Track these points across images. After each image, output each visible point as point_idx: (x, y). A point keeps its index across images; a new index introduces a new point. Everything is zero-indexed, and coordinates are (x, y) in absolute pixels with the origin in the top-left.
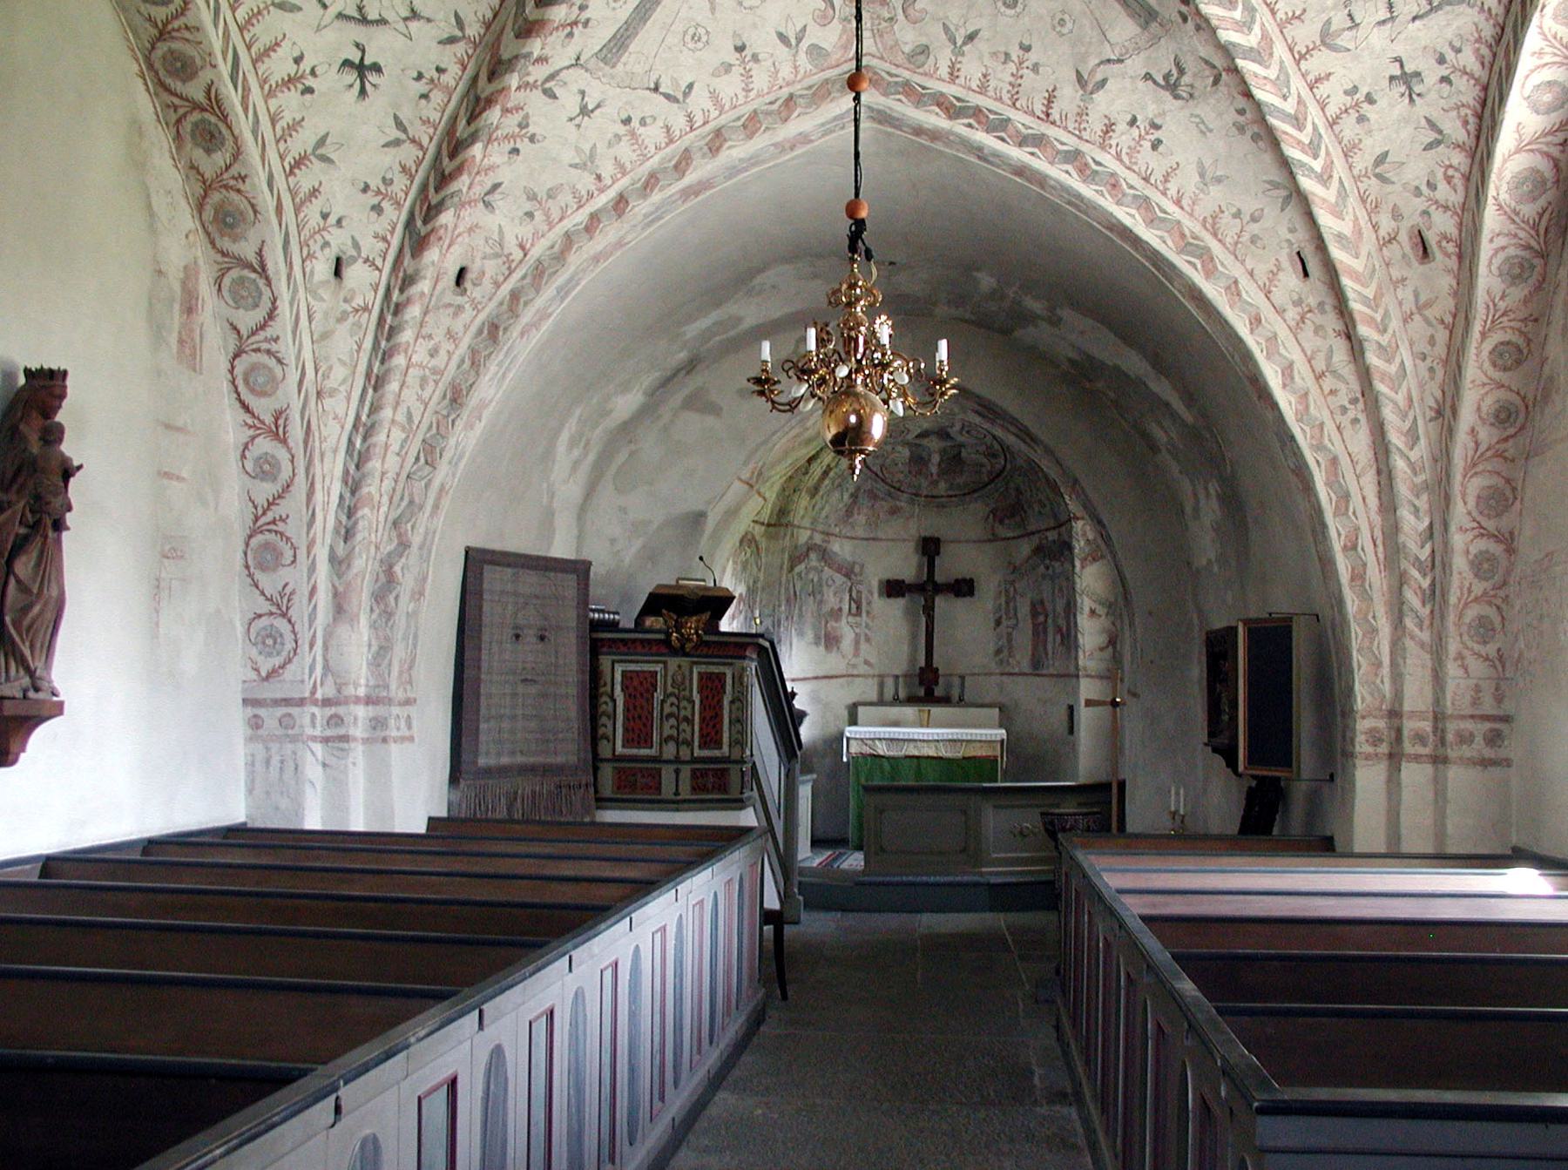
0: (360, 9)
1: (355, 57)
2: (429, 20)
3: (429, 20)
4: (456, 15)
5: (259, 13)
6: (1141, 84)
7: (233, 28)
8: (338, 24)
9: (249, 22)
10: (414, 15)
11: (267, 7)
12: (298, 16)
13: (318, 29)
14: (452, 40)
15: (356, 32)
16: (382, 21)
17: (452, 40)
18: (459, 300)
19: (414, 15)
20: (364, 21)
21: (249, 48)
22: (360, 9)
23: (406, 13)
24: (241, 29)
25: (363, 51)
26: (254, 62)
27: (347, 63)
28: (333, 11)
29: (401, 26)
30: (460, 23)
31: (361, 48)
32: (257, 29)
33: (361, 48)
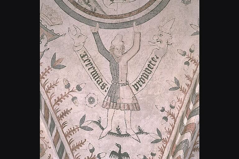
0: (118, 130)
1: (117, 150)
2: (147, 133)
3: (147, 133)
4: (158, 130)
5: (74, 130)
6: (79, 39)
7: (56, 120)
8: (110, 136)
9: (62, 116)
10: (141, 132)
11: (78, 128)
12: (92, 132)
13: (100, 138)
14: (157, 141)
15: (118, 140)
16: (128, 135)
17: (157, 141)
18: (68, 121)
19: (141, 132)
20: (119, 135)
21: (69, 144)
22: (118, 130)
23: (137, 131)
24: (66, 136)
25: (120, 148)
26: (72, 150)
27: (113, 153)
28: (106, 131)
29: (135, 136)
30: (159, 133)
31: (119, 146)
32: (73, 136)
33: (119, 146)
